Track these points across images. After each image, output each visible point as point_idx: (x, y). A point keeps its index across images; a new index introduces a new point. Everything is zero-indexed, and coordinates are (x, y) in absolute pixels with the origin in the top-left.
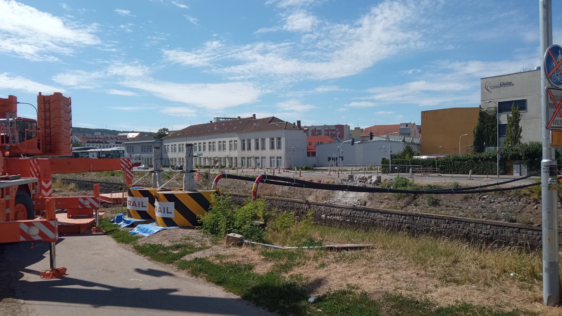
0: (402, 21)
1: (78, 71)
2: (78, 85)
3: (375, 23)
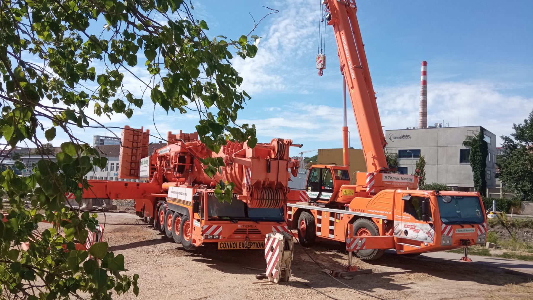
0: (267, 65)
3: (244, 64)
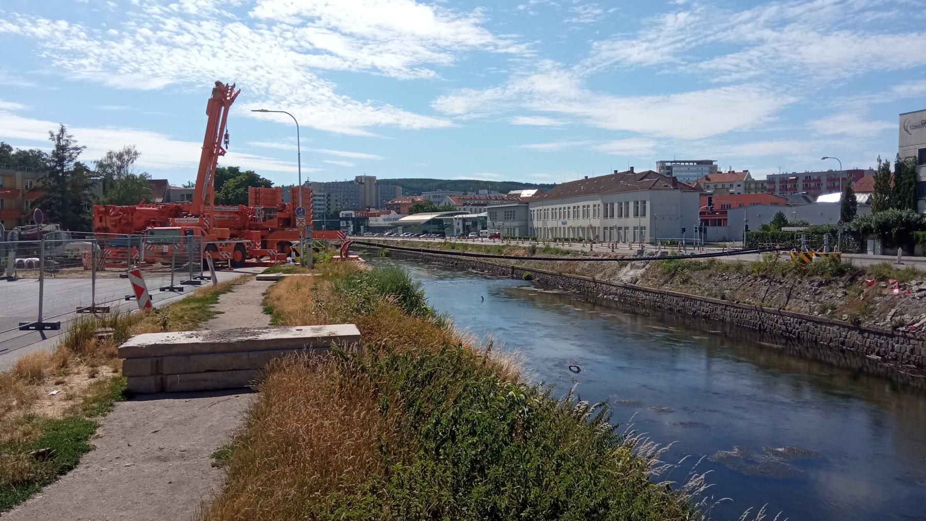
1: (464, 91)
2: (468, 113)
